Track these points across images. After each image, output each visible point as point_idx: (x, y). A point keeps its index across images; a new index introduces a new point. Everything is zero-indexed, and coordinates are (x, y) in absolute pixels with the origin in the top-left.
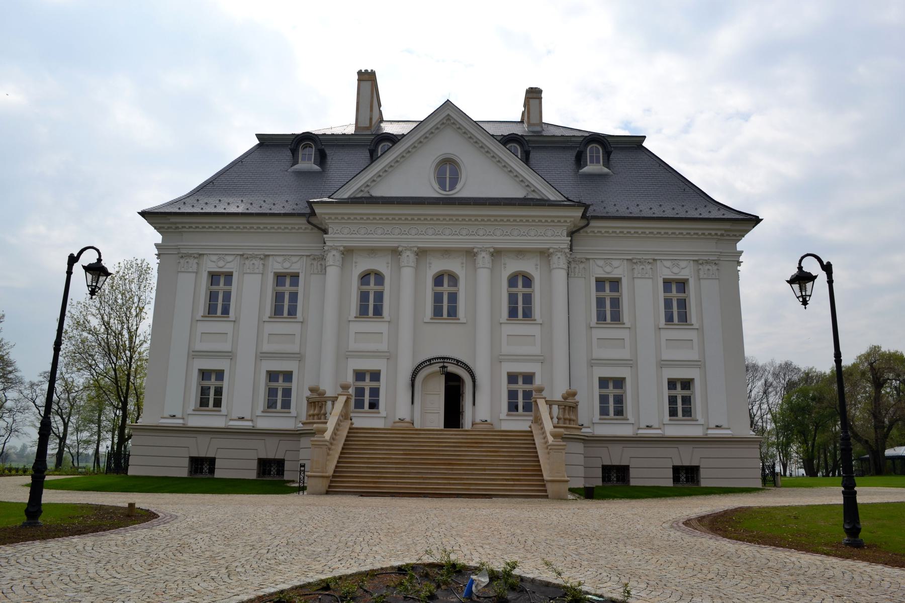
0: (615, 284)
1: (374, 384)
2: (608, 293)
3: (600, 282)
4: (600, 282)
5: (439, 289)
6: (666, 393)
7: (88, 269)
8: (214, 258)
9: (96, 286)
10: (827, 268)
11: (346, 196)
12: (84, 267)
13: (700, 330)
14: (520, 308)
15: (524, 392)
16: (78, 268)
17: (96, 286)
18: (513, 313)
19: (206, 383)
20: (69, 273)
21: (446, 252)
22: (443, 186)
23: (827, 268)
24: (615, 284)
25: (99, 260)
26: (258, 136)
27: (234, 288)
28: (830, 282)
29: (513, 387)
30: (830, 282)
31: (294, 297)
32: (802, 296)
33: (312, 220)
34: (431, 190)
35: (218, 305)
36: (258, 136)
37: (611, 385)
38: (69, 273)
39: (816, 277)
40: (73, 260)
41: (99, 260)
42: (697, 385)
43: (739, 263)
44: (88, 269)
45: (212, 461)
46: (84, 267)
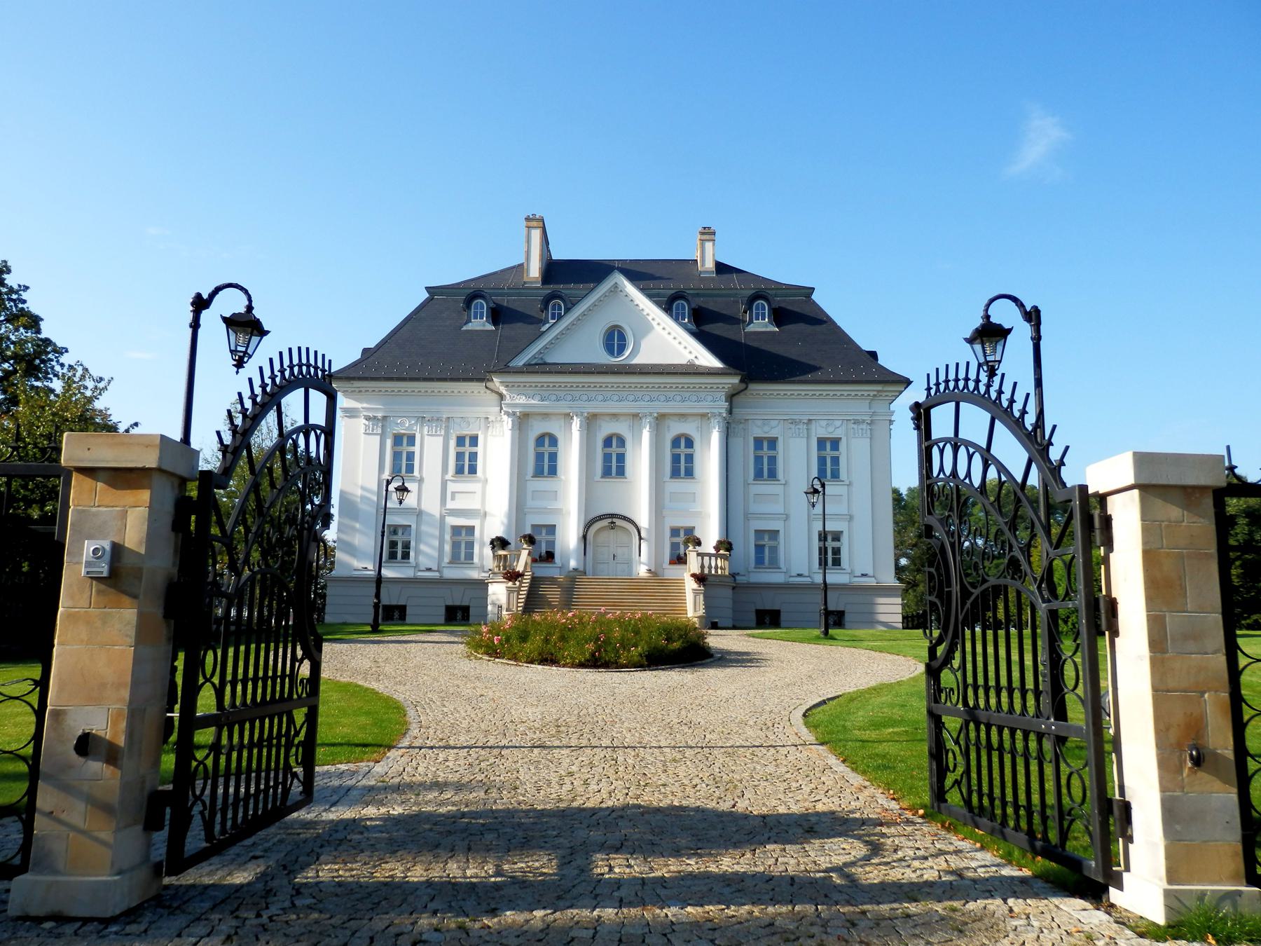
0: (773, 442)
1: (836, 544)
2: (765, 452)
3: (758, 442)
4: (758, 442)
5: (608, 450)
6: (816, 544)
7: (232, 322)
8: (824, 423)
9: (245, 353)
10: (1033, 317)
11: (521, 364)
12: (225, 319)
13: (421, 481)
14: (466, 465)
15: (686, 455)
16: (211, 318)
17: (245, 353)
18: (759, 475)
19: (457, 538)
20: (195, 325)
21: (615, 416)
22: (609, 348)
23: (1033, 317)
25: (250, 308)
27: (479, 449)
28: (1037, 340)
29: (676, 540)
30: (1037, 340)
31: (473, 456)
32: (987, 362)
33: (489, 384)
34: (602, 357)
35: (767, 470)
37: (766, 537)
38: (195, 325)
39: (1009, 331)
40: (200, 304)
41: (250, 308)
42: (845, 539)
43: (891, 422)
44: (232, 322)
46: (225, 319)
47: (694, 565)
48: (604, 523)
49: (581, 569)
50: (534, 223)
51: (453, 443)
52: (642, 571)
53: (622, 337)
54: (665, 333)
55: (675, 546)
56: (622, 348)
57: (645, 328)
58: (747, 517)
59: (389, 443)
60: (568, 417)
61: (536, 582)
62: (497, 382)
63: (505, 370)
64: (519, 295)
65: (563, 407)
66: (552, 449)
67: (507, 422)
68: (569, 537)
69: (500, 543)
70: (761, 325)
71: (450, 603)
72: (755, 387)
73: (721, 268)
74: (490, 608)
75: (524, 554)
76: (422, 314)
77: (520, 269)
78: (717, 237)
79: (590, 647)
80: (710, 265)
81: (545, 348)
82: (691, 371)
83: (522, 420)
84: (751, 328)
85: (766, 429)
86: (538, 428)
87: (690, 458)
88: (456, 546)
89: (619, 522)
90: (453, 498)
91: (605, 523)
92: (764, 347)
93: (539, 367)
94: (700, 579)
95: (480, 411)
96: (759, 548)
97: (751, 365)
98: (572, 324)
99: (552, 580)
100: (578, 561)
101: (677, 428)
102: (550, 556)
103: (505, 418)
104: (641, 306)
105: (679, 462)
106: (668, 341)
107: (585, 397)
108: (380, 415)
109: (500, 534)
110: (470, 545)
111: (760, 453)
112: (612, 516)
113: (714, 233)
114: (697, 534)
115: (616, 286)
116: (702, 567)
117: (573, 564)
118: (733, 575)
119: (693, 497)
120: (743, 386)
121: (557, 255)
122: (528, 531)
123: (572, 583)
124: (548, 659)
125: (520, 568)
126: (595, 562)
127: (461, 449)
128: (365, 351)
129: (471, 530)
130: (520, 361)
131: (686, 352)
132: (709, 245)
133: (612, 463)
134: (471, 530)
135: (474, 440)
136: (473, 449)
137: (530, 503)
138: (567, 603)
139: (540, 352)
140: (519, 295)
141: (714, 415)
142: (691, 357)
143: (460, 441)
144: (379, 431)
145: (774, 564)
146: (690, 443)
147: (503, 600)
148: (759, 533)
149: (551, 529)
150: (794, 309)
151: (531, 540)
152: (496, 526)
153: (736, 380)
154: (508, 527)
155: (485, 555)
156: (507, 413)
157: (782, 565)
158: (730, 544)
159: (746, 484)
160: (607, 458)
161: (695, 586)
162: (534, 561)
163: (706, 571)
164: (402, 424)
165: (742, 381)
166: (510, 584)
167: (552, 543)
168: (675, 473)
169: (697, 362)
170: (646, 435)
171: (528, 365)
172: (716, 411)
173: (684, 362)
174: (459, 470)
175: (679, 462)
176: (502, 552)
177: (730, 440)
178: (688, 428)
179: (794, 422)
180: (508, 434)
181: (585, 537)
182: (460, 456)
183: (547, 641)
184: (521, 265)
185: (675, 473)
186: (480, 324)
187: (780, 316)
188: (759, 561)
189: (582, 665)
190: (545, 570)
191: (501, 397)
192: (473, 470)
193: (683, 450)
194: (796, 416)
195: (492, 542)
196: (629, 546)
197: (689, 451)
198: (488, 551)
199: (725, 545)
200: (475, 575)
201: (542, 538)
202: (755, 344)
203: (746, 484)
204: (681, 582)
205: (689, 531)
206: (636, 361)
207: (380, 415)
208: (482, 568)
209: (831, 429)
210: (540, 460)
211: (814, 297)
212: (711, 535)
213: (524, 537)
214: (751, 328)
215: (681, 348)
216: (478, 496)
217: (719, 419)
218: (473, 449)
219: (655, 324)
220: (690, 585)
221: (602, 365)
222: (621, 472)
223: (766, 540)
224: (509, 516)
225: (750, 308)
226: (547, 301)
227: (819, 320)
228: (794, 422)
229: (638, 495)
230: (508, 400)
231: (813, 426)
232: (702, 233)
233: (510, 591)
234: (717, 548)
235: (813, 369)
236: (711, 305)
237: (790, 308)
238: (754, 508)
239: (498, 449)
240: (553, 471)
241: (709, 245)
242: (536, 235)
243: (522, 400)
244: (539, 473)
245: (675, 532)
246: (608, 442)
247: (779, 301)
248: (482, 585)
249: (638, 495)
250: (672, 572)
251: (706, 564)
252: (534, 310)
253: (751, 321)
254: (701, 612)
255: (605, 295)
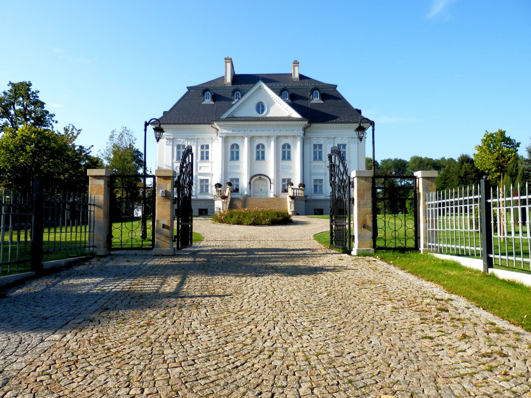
3: (315, 146)
4: (315, 146)
5: (258, 150)
8: (340, 138)
11: (225, 117)
18: (315, 159)
21: (260, 137)
22: (258, 111)
24: (320, 146)
26: (187, 87)
27: (210, 150)
31: (207, 153)
33: (213, 125)
34: (256, 114)
36: (187, 87)
37: (318, 182)
45: (207, 210)
47: (290, 193)
48: (257, 177)
49: (249, 194)
50: (228, 61)
51: (199, 148)
52: (271, 195)
53: (263, 107)
54: (279, 105)
55: (284, 186)
56: (263, 111)
57: (272, 103)
58: (311, 174)
59: (175, 148)
60: (243, 138)
61: (232, 200)
62: (216, 124)
63: (219, 120)
64: (223, 89)
65: (241, 134)
66: (237, 150)
67: (220, 140)
68: (244, 183)
69: (218, 185)
70: (317, 100)
71: (200, 208)
72: (314, 125)
73: (302, 77)
74: (215, 209)
75: (228, 190)
76: (186, 98)
77: (223, 78)
78: (300, 65)
79: (253, 219)
80: (297, 76)
81: (234, 111)
82: (289, 119)
83: (226, 139)
84: (312, 102)
85: (318, 141)
86: (232, 142)
87: (289, 153)
88: (202, 186)
89: (262, 177)
90: (200, 169)
91: (258, 177)
92: (317, 109)
93: (232, 119)
94: (292, 198)
95: (209, 136)
96: (316, 186)
97: (312, 116)
98: (244, 102)
99: (238, 199)
100: (248, 192)
101: (284, 141)
102: (237, 190)
103: (219, 138)
104: (270, 94)
105: (285, 154)
106: (281, 108)
107: (249, 130)
108: (171, 138)
109: (218, 182)
110: (207, 186)
111: (316, 150)
112: (260, 175)
113: (298, 63)
114: (292, 181)
115: (260, 86)
116: (294, 193)
117: (246, 193)
118: (305, 196)
119: (290, 167)
120: (309, 125)
121: (236, 73)
122: (229, 181)
123: (245, 201)
124: (239, 223)
125: (226, 195)
126: (254, 192)
127: (203, 150)
128: (165, 113)
129: (207, 181)
130: (224, 116)
131: (287, 112)
132: (296, 68)
133: (259, 155)
134: (207, 181)
135: (207, 147)
136: (207, 150)
137: (229, 170)
138: (244, 205)
139: (231, 113)
140: (223, 89)
141: (298, 136)
142: (289, 114)
143: (202, 147)
144: (172, 144)
145: (321, 192)
146: (289, 147)
147: (221, 206)
148: (315, 181)
149: (237, 180)
150: (330, 94)
151: (230, 184)
152: (216, 179)
153: (306, 123)
154: (221, 179)
155: (213, 190)
156: (220, 136)
157: (324, 192)
158: (304, 185)
159: (311, 162)
160: (258, 153)
161: (291, 200)
162: (231, 192)
163: (295, 195)
164: (180, 141)
165: (308, 123)
166: (223, 200)
167: (238, 185)
168: (284, 158)
169: (292, 116)
170: (272, 144)
171: (227, 118)
172: (299, 135)
173: (287, 116)
174: (202, 158)
175: (285, 154)
176: (219, 189)
177: (305, 145)
178: (288, 141)
179: (328, 138)
180: (220, 145)
181: (250, 183)
182: (202, 153)
183: (239, 218)
184: (223, 77)
185: (284, 158)
186: (208, 101)
187: (324, 97)
188: (316, 191)
189: (250, 225)
190: (235, 195)
191: (217, 130)
192: (207, 158)
193: (286, 150)
194: (330, 136)
195: (216, 185)
196: (267, 186)
197: (289, 150)
198: (214, 189)
199: (302, 185)
200: (209, 197)
201: (234, 183)
202: (314, 108)
203: (311, 162)
204: (286, 199)
205: (289, 180)
206: (268, 116)
207: (171, 138)
208: (212, 195)
209: (343, 141)
210: (233, 154)
211: (337, 89)
212: (297, 181)
213: (228, 183)
214: (312, 102)
215: (285, 110)
216: (210, 168)
217: (300, 137)
218: (207, 150)
219: (275, 101)
220: (289, 200)
221: (255, 118)
222: (263, 158)
223: (318, 183)
224: (222, 176)
225: (312, 94)
226: (234, 92)
227: (339, 98)
228: (328, 138)
229: (269, 167)
230: (220, 131)
231: (336, 139)
232: (294, 63)
233: (223, 203)
234: (299, 186)
235: (336, 118)
236: (297, 93)
237: (327, 93)
238: (314, 171)
239: (216, 149)
240: (238, 158)
241: (296, 68)
242: (229, 65)
243: (225, 131)
244: (232, 159)
245: (284, 180)
246: (258, 147)
247: (323, 91)
248: (212, 201)
249: (269, 167)
250: (283, 195)
251: (295, 192)
252: (229, 95)
253: (313, 99)
254: (293, 209)
255: (256, 90)
